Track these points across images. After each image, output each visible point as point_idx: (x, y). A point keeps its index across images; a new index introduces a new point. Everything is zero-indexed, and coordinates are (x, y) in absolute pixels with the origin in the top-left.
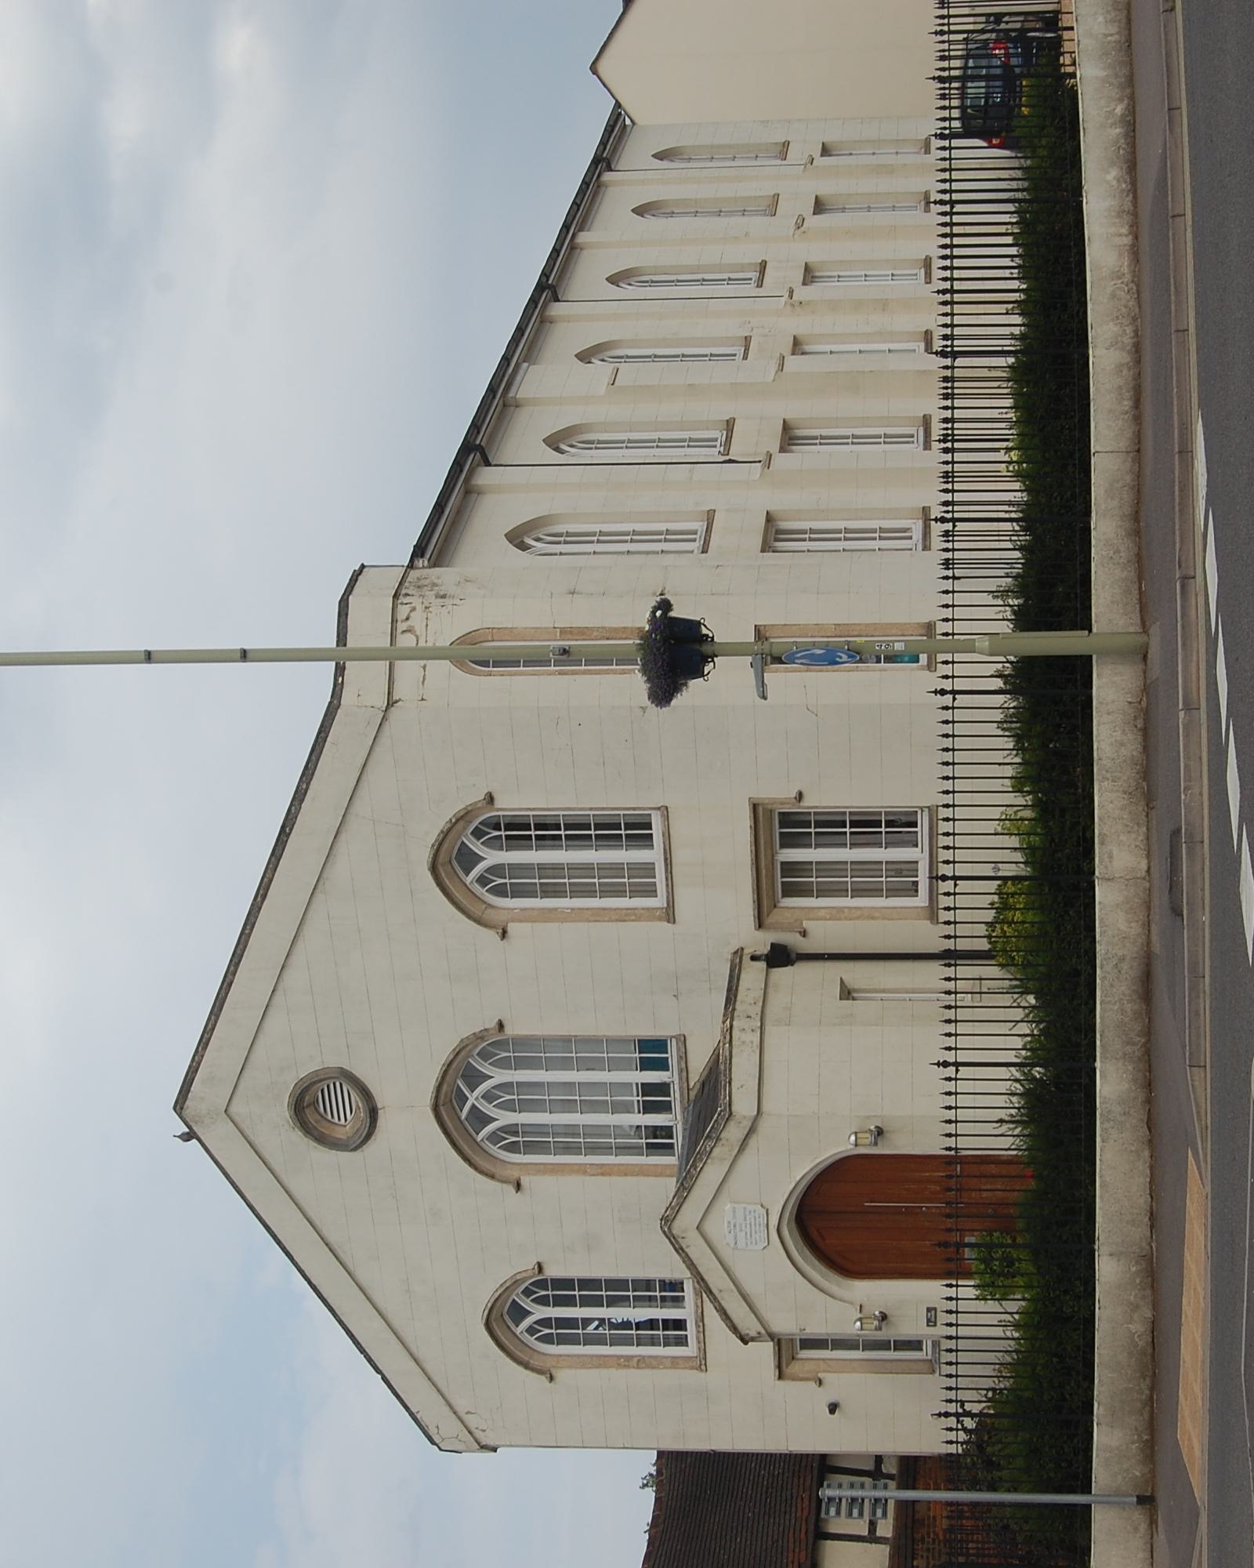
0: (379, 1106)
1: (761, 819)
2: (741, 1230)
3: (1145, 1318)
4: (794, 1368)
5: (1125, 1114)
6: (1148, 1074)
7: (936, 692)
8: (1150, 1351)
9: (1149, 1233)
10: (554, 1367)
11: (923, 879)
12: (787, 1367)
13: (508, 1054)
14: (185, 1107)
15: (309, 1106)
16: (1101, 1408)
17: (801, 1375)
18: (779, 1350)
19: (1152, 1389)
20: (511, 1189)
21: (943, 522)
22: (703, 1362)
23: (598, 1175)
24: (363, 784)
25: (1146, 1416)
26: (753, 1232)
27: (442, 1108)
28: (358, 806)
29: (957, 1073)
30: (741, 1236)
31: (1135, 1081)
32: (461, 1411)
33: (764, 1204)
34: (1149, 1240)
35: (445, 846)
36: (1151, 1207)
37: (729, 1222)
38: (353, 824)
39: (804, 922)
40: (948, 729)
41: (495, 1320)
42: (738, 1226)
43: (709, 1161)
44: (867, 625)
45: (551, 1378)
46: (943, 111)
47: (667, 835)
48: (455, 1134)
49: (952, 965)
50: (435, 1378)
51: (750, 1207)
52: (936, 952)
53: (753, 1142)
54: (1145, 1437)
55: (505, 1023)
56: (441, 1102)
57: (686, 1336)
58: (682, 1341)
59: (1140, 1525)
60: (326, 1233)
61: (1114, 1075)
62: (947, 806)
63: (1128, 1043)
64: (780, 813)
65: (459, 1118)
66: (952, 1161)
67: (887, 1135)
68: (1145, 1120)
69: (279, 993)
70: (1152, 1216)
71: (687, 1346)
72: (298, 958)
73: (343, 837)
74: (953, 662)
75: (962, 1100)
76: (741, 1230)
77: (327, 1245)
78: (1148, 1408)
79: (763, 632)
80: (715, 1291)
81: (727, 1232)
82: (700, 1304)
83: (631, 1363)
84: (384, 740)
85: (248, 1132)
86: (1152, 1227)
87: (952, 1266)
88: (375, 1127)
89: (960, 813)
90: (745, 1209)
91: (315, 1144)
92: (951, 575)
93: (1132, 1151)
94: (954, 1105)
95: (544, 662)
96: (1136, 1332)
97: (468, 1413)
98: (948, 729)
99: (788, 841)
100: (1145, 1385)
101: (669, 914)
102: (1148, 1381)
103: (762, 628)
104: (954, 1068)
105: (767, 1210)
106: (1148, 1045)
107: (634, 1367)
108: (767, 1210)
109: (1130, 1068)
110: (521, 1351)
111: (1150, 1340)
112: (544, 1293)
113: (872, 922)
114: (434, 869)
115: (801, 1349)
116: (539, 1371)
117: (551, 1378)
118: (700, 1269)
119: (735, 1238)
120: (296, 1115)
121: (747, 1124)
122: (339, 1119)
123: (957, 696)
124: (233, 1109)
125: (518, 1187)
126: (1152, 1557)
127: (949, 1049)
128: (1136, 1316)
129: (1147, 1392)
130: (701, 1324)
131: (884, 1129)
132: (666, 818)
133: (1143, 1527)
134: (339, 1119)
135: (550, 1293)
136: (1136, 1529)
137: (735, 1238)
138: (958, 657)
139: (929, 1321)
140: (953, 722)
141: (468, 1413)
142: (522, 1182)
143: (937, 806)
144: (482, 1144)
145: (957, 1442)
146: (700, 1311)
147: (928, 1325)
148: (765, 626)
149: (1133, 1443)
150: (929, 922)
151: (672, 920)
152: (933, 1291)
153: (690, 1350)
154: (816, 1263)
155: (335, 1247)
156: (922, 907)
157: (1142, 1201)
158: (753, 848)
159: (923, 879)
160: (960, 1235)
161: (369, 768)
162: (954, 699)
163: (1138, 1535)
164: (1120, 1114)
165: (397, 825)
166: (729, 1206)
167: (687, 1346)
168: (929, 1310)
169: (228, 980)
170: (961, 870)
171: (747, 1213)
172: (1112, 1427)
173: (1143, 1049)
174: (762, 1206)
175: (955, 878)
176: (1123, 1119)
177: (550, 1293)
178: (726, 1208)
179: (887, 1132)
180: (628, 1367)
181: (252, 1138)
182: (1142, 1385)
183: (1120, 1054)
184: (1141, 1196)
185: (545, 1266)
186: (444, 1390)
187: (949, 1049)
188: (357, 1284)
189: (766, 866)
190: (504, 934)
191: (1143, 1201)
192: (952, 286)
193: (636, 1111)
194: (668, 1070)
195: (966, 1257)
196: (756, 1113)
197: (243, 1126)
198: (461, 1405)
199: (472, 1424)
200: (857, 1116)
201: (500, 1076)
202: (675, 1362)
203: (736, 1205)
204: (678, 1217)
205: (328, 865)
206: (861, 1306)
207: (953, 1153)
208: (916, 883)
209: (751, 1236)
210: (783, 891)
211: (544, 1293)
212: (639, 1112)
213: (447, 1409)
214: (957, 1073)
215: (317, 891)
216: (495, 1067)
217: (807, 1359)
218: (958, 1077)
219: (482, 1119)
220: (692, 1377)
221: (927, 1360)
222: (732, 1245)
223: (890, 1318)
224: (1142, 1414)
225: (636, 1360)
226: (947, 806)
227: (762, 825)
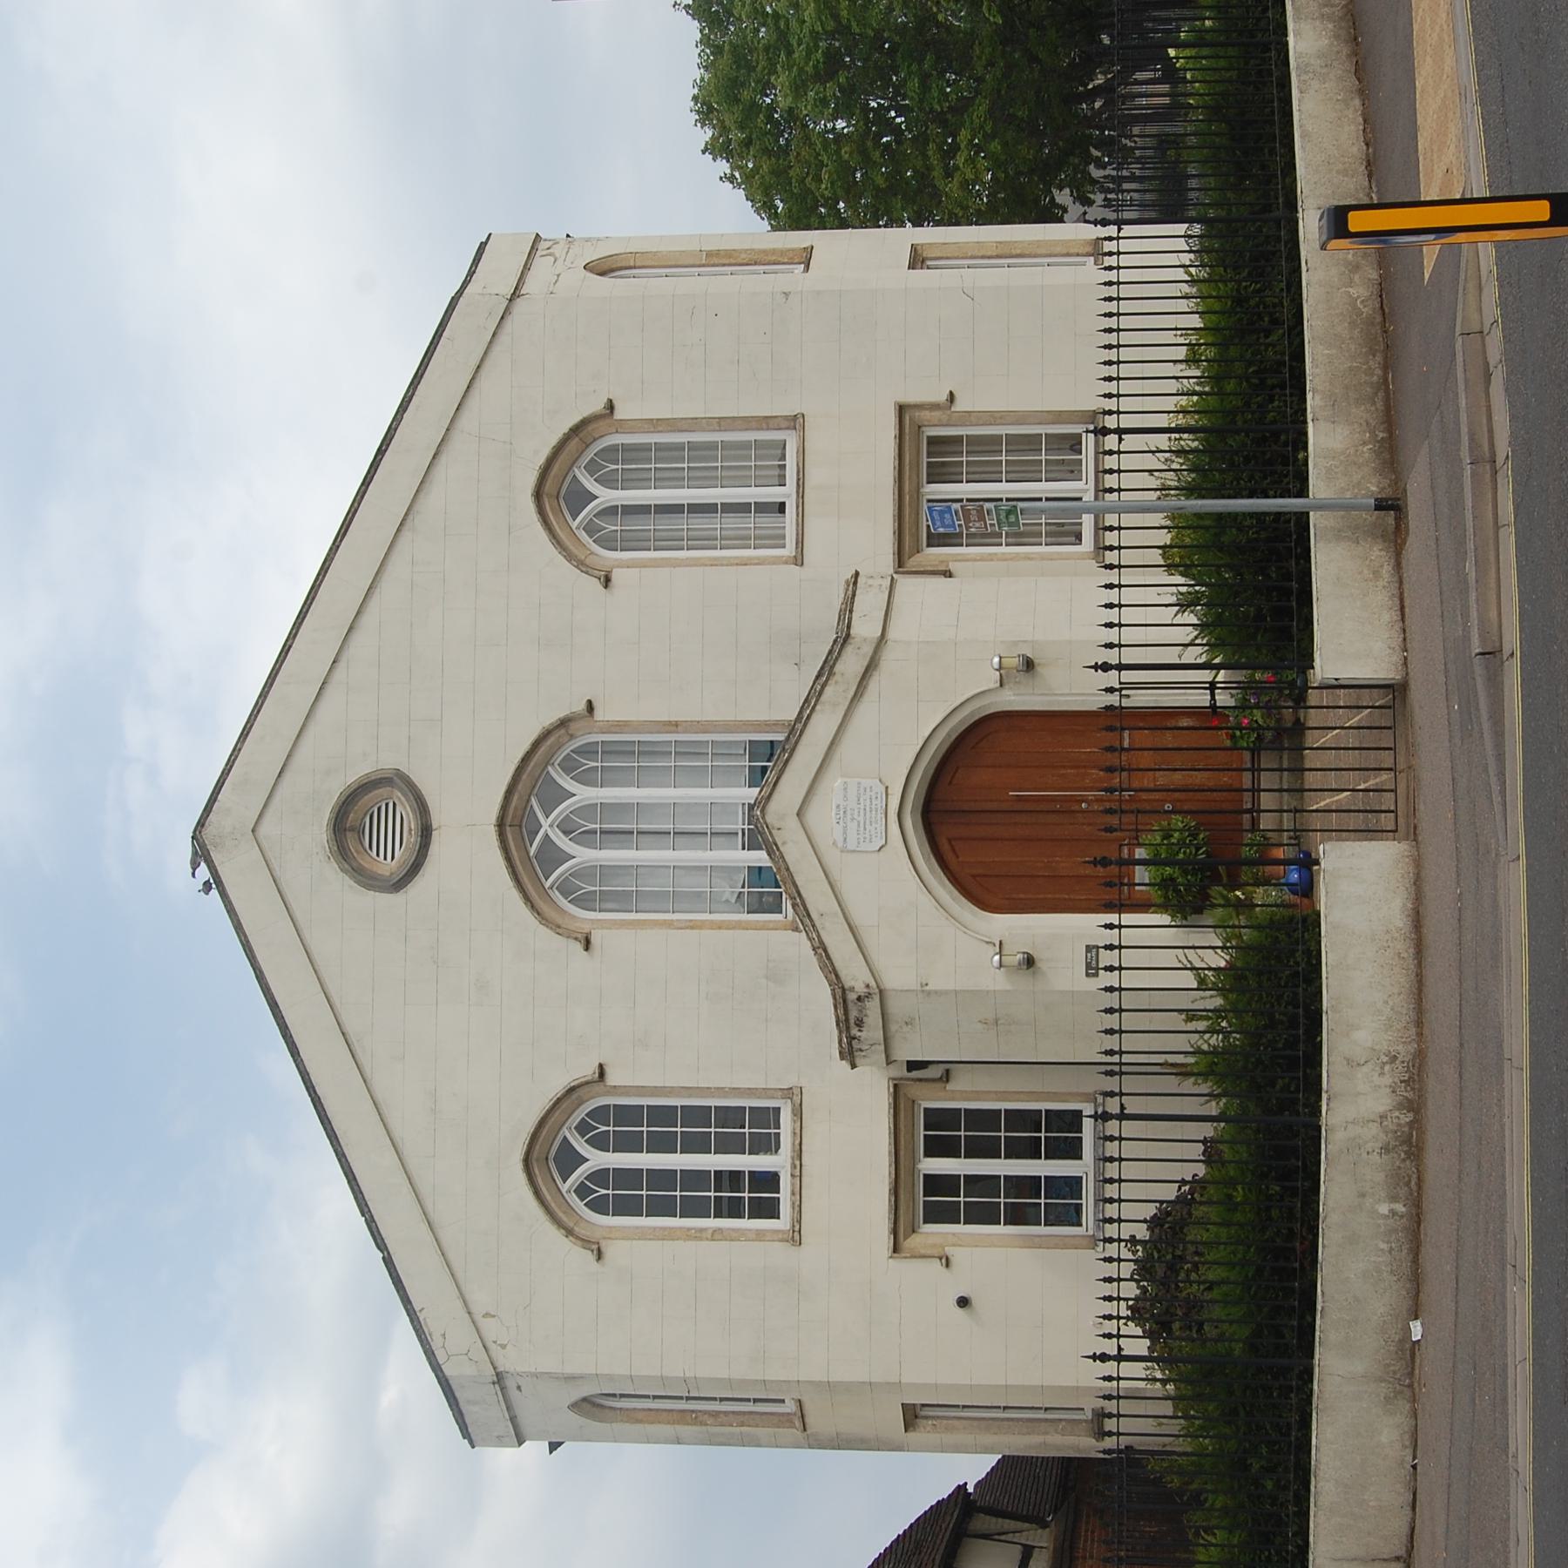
0: (434, 827)
1: (907, 431)
2: (853, 819)
3: (1369, 279)
4: (913, 1242)
5: (1326, 66)
6: (1352, 31)
7: (1096, 667)
8: (1379, 319)
9: (1367, 183)
10: (604, 1238)
11: (1088, 522)
12: (905, 1239)
13: (607, 1128)
14: (207, 824)
15: (352, 829)
16: (1317, 397)
17: (923, 1252)
18: (896, 1201)
19: (1386, 367)
20: (579, 947)
21: (1104, 225)
22: (797, 1228)
23: (687, 928)
24: (475, 392)
25: (1380, 405)
26: (868, 822)
27: (508, 829)
28: (465, 421)
29: (1119, 232)
30: (852, 826)
31: (1337, 37)
32: (478, 1310)
33: (883, 780)
34: (1367, 190)
35: (555, 470)
36: (1367, 155)
37: (838, 806)
38: (457, 438)
39: (950, 564)
40: (1113, 615)
41: (537, 1160)
42: (849, 812)
43: (818, 707)
44: (1030, 243)
45: (599, 1255)
46: (1109, 755)
47: (799, 1135)
48: (520, 868)
49: (1116, 1074)
50: (451, 1255)
51: (866, 783)
52: (1095, 709)
53: (873, 685)
54: (1381, 435)
55: (595, 704)
56: (508, 820)
57: (779, 1198)
58: (774, 1214)
59: (1382, 566)
60: (344, 1018)
61: (1311, 33)
62: (1110, 947)
63: (1326, 6)
64: (925, 1109)
65: (528, 853)
66: (1114, 718)
67: (1038, 669)
68: (1353, 70)
69: (342, 665)
70: (1370, 164)
71: (779, 1218)
72: (368, 620)
73: (443, 459)
74: (1120, 927)
75: (1128, 615)
76: (853, 819)
77: (343, 1034)
78: (1381, 394)
79: (920, 252)
80: (814, 916)
81: (835, 821)
82: (798, 1131)
83: (704, 1235)
84: (504, 338)
85: (275, 864)
86: (1370, 176)
87: (1111, 895)
88: (425, 856)
89: (1129, 958)
90: (859, 783)
91: (352, 883)
92: (1116, 1110)
93: (1338, 100)
94: (1116, 1197)
95: (695, 900)
96: (1358, 297)
97: (487, 1315)
98: (1113, 615)
99: (938, 474)
100: (1375, 363)
101: (799, 560)
102: (1379, 358)
103: (919, 248)
104: (1116, 227)
105: (887, 788)
106: (1350, 7)
107: (707, 1239)
108: (887, 788)
109: (1330, 26)
110: (564, 1213)
111: (1378, 306)
112: (604, 1192)
113: (1029, 562)
114: (538, 495)
115: (925, 1222)
116: (586, 1243)
117: (599, 1255)
118: (796, 878)
119: (845, 833)
120: (335, 833)
121: (868, 650)
122: (378, 855)
123: (1123, 436)
124: (263, 830)
125: (587, 944)
126: (1403, 620)
127: (1109, 396)
128: (1356, 278)
129: (1379, 372)
130: (798, 1163)
131: (1036, 661)
132: (798, 1113)
133: (1387, 570)
134: (378, 855)
135: (611, 1128)
136: (1376, 574)
137: (845, 833)
138: (1127, 918)
139: (1088, 966)
140: (1120, 606)
141: (487, 1315)
142: (593, 940)
143: (1098, 947)
144: (550, 892)
145: (1119, 1299)
146: (798, 1142)
147: (1088, 975)
148: (922, 245)
149: (1364, 443)
150: (1094, 1440)
151: (799, 562)
152: (1088, 926)
153: (783, 1223)
154: (947, 882)
155: (353, 1039)
156: (1086, 1421)
157: (1355, 149)
158: (897, 462)
159: (1088, 522)
160: (1129, 850)
161: (483, 372)
162: (1120, 440)
163: (1381, 583)
164: (1321, 67)
165: (505, 442)
166: (839, 782)
167: (779, 1218)
168: (1089, 948)
169: (289, 643)
170: (1127, 422)
171: (862, 790)
172: (1334, 422)
173: (1345, 9)
174: (880, 781)
175: (1120, 432)
176: (1324, 70)
177: (610, 1192)
178: (836, 784)
179: (1039, 664)
180: (701, 1239)
181: (277, 873)
182: (1371, 363)
183: (1317, 14)
184: (1353, 144)
185: (608, 1070)
186: (460, 1275)
187: (1109, 396)
188: (372, 1098)
189: (910, 491)
190: (607, 581)
191: (1356, 149)
192: (1120, 1349)
193: (740, 846)
194: (781, 912)
195: (1137, 881)
196: (879, 634)
197: (269, 855)
198: (481, 1300)
199: (490, 1336)
200: (1002, 642)
201: (584, 794)
202: (760, 1235)
203: (848, 780)
204: (776, 796)
205: (422, 495)
206: (1001, 943)
207: (1116, 1058)
208: (1078, 1208)
209: (865, 829)
210: (928, 475)
211: (604, 1192)
212: (744, 849)
213: (459, 1303)
214: (1119, 232)
215: (406, 528)
216: (577, 843)
217: (932, 1233)
218: (1120, 235)
219: (551, 857)
220: (780, 1253)
221: (1088, 1236)
222: (840, 844)
223: (1039, 964)
224: (1374, 403)
225: (710, 1232)
226: (1110, 947)
227: (907, 438)
